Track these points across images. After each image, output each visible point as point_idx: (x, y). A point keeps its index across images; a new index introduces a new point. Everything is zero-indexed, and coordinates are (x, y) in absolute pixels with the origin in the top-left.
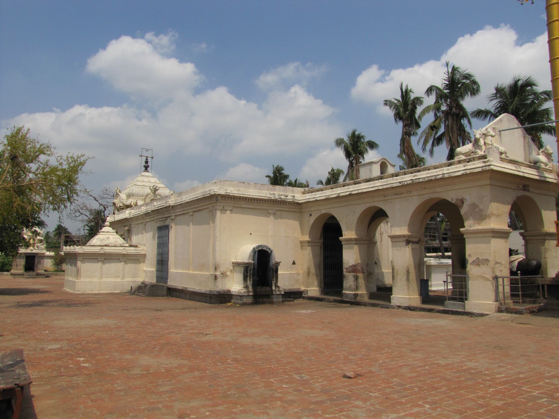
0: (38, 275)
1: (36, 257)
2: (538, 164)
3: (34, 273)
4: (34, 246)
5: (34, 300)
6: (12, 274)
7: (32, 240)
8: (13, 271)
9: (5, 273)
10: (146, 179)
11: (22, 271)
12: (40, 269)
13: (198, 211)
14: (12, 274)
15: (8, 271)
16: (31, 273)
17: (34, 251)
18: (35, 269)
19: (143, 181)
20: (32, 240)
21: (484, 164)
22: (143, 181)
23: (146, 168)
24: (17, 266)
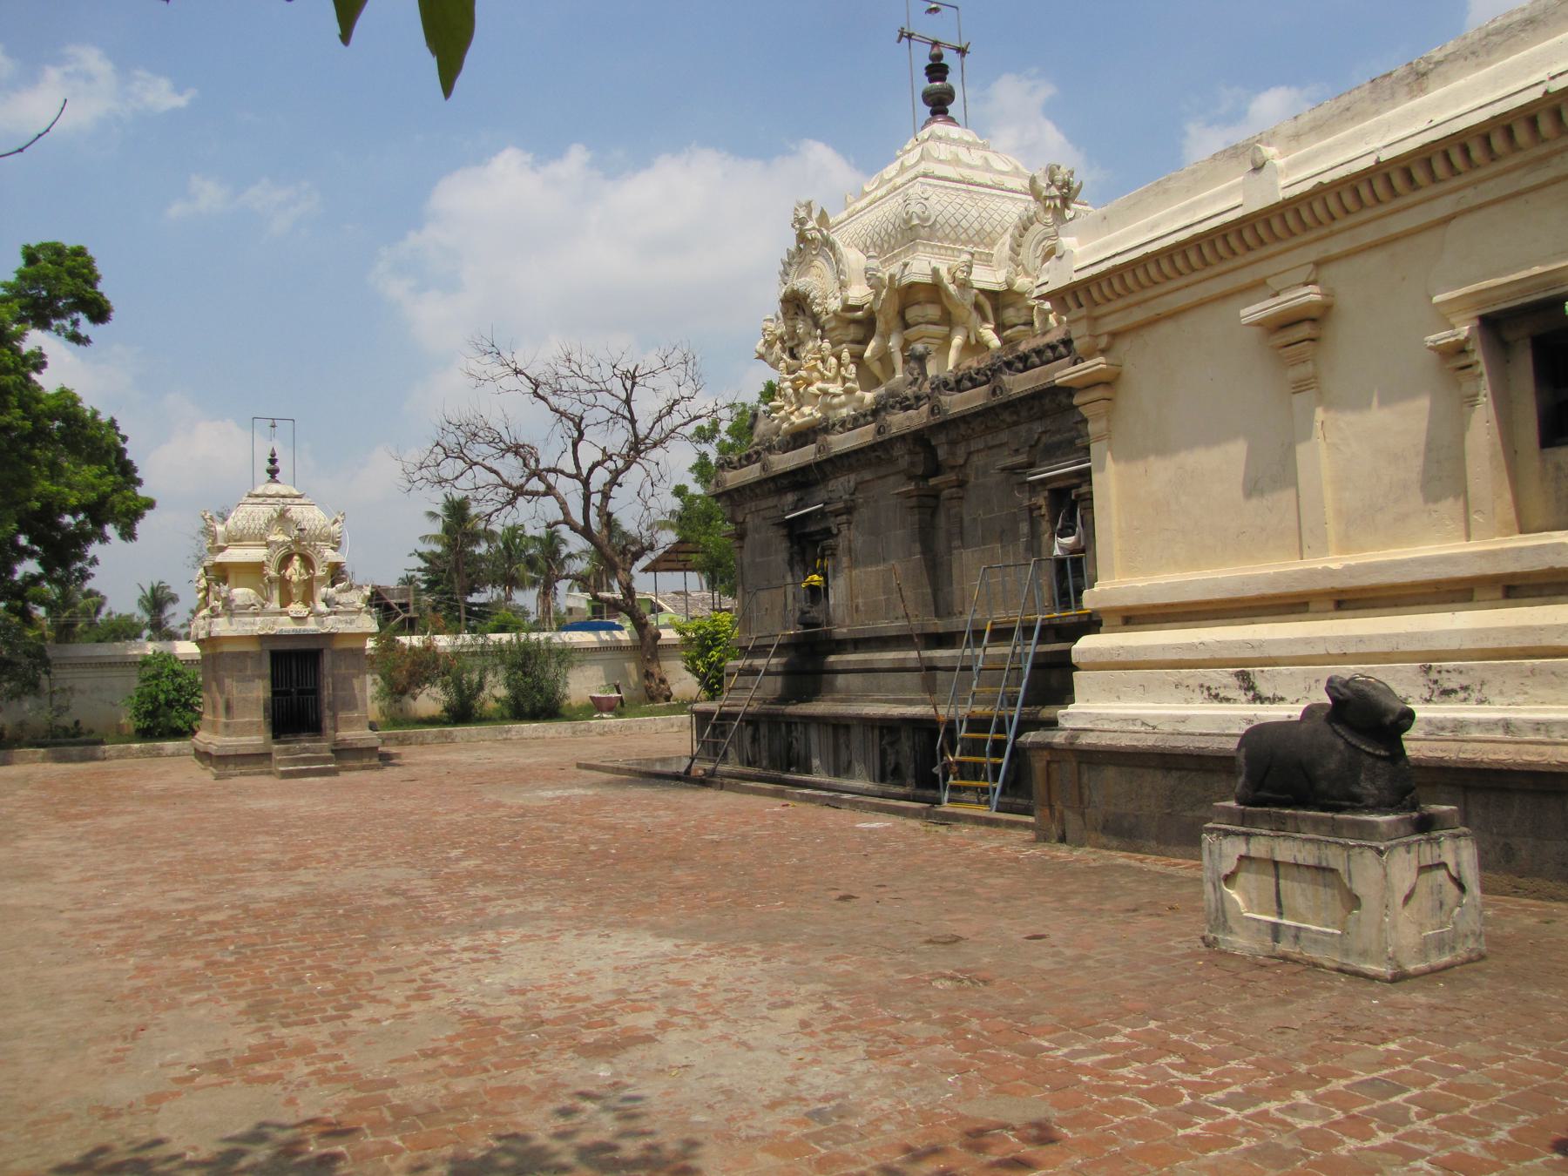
0: (347, 754)
1: (327, 661)
2: (761, 426)
3: (323, 746)
4: (308, 599)
5: (773, 806)
6: (204, 756)
7: (296, 562)
8: (205, 738)
9: (170, 745)
10: (942, 151)
11: (257, 739)
12: (350, 723)
13: (1201, 304)
14: (204, 756)
15: (178, 734)
16: (305, 745)
17: (312, 626)
18: (327, 723)
19: (956, 162)
20: (296, 562)
21: (377, 871)
22: (956, 162)
23: (939, 104)
24: (228, 708)
